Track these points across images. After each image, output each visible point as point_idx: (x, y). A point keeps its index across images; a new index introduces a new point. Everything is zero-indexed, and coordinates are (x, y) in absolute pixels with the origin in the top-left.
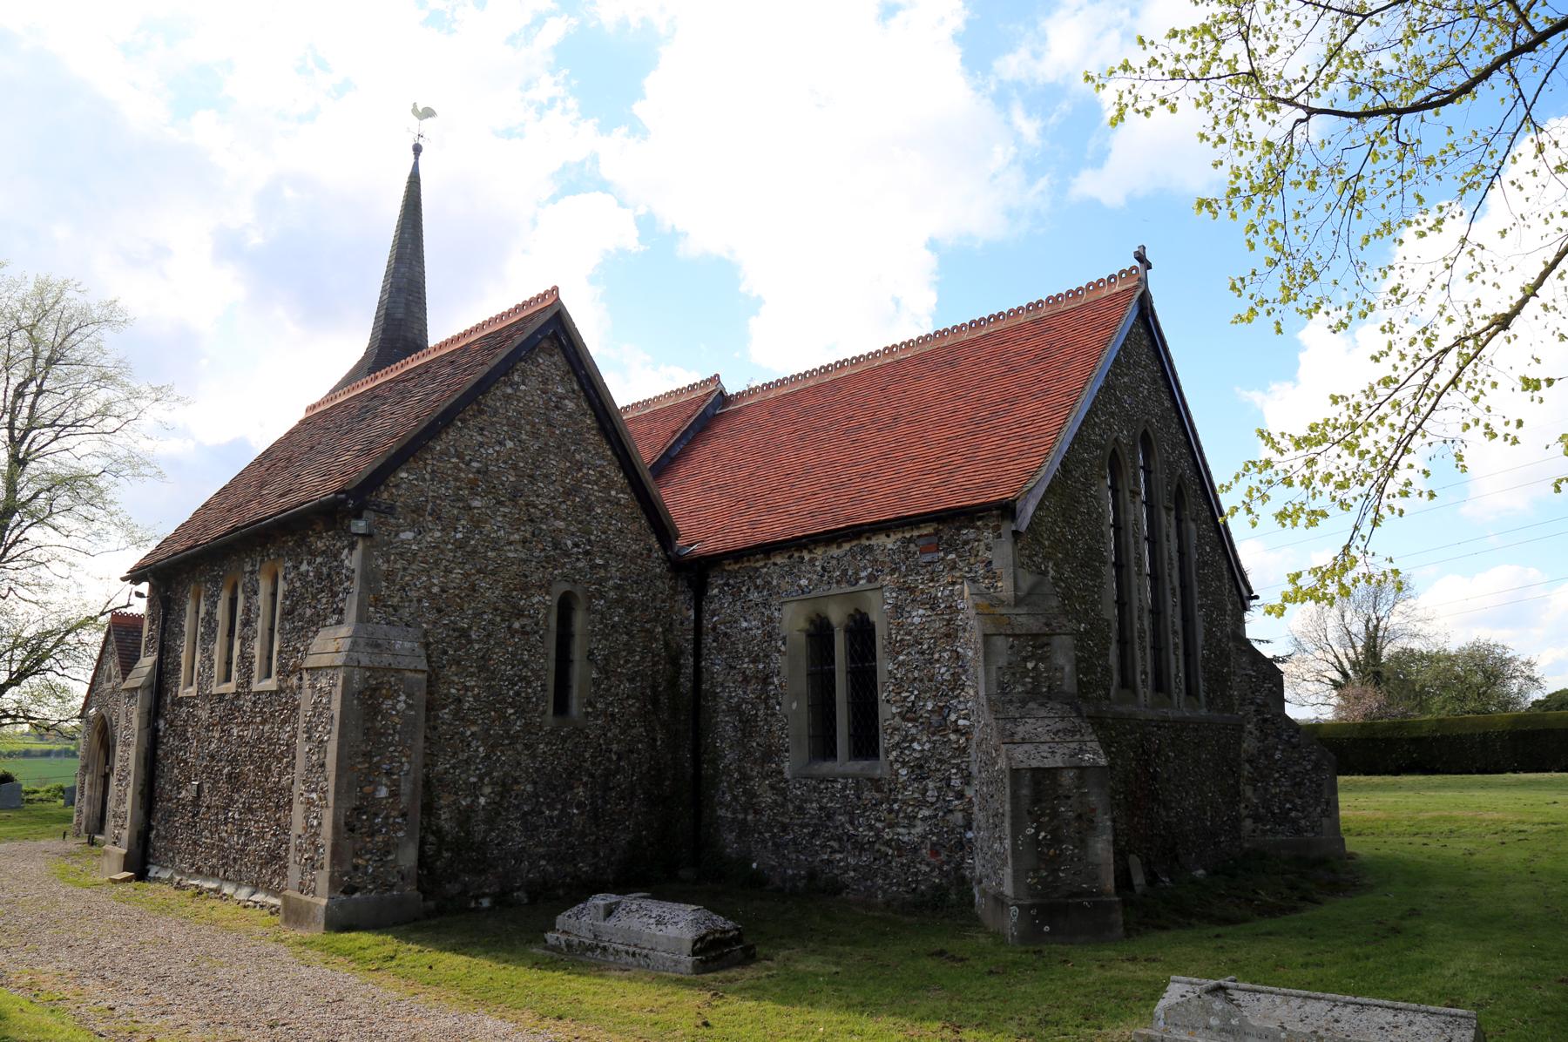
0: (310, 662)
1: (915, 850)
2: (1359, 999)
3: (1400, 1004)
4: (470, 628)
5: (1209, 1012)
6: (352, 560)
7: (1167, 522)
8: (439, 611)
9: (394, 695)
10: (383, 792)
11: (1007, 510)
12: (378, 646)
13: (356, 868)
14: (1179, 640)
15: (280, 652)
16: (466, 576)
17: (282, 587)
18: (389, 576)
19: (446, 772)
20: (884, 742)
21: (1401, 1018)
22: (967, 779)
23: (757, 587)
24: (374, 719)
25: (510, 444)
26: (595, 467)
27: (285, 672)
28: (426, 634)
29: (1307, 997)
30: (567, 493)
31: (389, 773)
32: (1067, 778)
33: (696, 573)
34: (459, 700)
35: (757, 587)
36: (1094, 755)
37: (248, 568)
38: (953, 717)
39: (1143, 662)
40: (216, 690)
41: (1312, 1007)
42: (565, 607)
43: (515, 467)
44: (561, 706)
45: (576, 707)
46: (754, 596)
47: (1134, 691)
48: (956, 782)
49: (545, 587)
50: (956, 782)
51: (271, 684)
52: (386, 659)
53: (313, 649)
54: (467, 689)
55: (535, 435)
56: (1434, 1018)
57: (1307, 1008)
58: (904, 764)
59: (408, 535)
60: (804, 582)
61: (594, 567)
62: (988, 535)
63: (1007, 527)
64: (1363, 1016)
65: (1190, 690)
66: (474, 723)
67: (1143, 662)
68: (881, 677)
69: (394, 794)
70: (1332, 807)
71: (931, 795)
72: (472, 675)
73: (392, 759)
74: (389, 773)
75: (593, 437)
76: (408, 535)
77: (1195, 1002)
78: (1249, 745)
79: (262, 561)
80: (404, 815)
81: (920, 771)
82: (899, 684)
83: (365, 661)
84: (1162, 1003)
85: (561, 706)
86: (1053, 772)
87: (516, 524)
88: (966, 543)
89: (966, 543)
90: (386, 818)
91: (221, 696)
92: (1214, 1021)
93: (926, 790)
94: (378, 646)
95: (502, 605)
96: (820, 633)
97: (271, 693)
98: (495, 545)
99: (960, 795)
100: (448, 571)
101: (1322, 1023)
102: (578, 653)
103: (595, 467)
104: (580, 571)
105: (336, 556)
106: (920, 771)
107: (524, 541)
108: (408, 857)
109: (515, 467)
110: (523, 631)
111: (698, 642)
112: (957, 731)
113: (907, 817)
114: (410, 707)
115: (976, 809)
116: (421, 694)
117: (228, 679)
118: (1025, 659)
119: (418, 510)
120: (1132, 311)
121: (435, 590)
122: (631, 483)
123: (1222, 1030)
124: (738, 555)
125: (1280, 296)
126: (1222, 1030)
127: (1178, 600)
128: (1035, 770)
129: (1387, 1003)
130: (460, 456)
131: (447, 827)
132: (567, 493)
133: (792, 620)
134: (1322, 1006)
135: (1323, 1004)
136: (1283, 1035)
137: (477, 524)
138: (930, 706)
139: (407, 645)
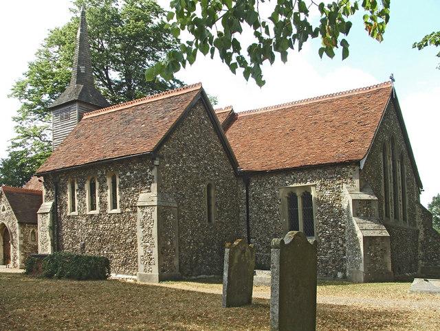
0: (138, 204)
1: (327, 262)
6: (154, 173)
7: (398, 165)
10: (169, 243)
11: (358, 163)
14: (401, 203)
15: (120, 201)
16: (183, 178)
17: (118, 181)
18: (164, 178)
20: (316, 231)
22: (344, 241)
23: (269, 183)
24: (165, 221)
25: (191, 136)
26: (214, 143)
27: (123, 207)
30: (207, 152)
33: (248, 177)
34: (184, 217)
35: (269, 183)
36: (386, 234)
37: (99, 173)
38: (340, 223)
39: (391, 209)
40: (89, 212)
42: (209, 187)
43: (193, 143)
44: (210, 220)
45: (213, 221)
46: (268, 186)
47: (389, 217)
48: (341, 242)
49: (203, 182)
50: (341, 242)
51: (118, 211)
53: (139, 200)
55: (197, 132)
58: (323, 237)
59: (168, 165)
60: (287, 182)
61: (216, 175)
62: (351, 170)
63: (357, 168)
65: (404, 219)
67: (391, 209)
68: (314, 212)
69: (171, 244)
71: (332, 246)
75: (212, 132)
76: (168, 165)
78: (421, 237)
79: (107, 171)
81: (328, 239)
82: (322, 214)
85: (210, 220)
87: (194, 162)
88: (344, 172)
89: (344, 172)
91: (92, 215)
93: (331, 244)
96: (292, 198)
97: (118, 214)
98: (189, 168)
99: (342, 246)
100: (179, 176)
102: (213, 203)
103: (214, 143)
104: (212, 177)
105: (145, 170)
106: (328, 239)
107: (197, 167)
108: (176, 262)
109: (193, 143)
110: (198, 196)
111: (247, 200)
112: (341, 227)
113: (324, 252)
115: (347, 250)
116: (176, 213)
117: (74, 210)
118: (364, 207)
119: (169, 157)
120: (388, 98)
122: (224, 148)
124: (262, 174)
127: (401, 190)
130: (178, 139)
132: (207, 152)
133: (282, 194)
137: (184, 162)
138: (332, 220)
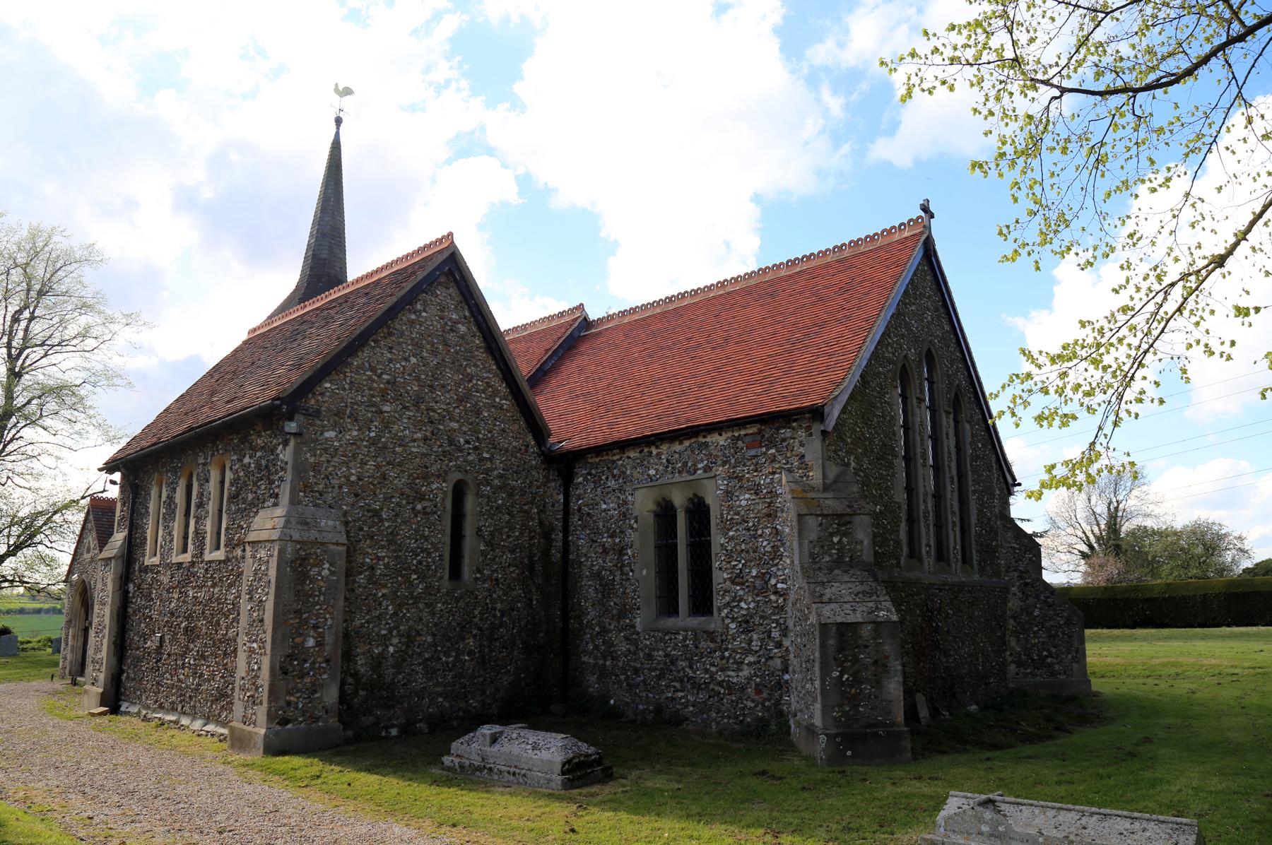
0: (252, 537)
1: (743, 689)
2: (1102, 810)
3: (1136, 814)
4: (381, 509)
5: (981, 821)
6: (286, 454)
7: (947, 423)
8: (356, 495)
9: (319, 564)
10: (311, 642)
11: (817, 413)
12: (306, 524)
13: (289, 704)
14: (957, 519)
15: (227, 529)
16: (378, 467)
17: (229, 476)
18: (316, 467)
19: (362, 626)
20: (718, 602)
21: (1137, 825)
22: (785, 632)
23: (614, 476)
24: (303, 583)
25: (413, 360)
26: (482, 379)
27: (231, 545)
28: (345, 514)
29: (1060, 809)
30: (460, 400)
31: (315, 627)
32: (866, 631)
33: (565, 465)
34: (372, 568)
35: (614, 476)
36: (887, 613)
37: (201, 461)
38: (773, 581)
39: (927, 537)
40: (175, 559)
41: (1064, 817)
42: (459, 492)
43: (418, 379)
44: (455, 572)
45: (467, 573)
46: (612, 483)
47: (920, 560)
48: (776, 634)
49: (442, 476)
50: (776, 634)
51: (220, 555)
52: (313, 534)
53: (254, 526)
54: (379, 559)
55: (434, 353)
56: (1163, 826)
57: (1060, 817)
58: (733, 620)
59: (331, 434)
60: (652, 472)
61: (482, 460)
62: (801, 434)
63: (817, 428)
64: (1106, 824)
65: (966, 560)
66: (385, 586)
67: (927, 537)
68: (715, 549)
69: (319, 644)
70: (1080, 655)
71: (755, 645)
72: (383, 547)
73: (318, 616)
74: (315, 627)
75: (481, 355)
76: (331, 434)
77: (970, 813)
78: (1013, 604)
79: (213, 455)
80: (327, 661)
81: (746, 625)
82: (729, 555)
83: (296, 536)
84: (942, 814)
85: (455, 572)
86: (854, 626)
87: (418, 425)
88: (784, 440)
89: (784, 440)
90: (313, 663)
91: (180, 565)
92: (985, 828)
93: (751, 641)
94: (306, 524)
95: (407, 491)
96: (665, 513)
97: (220, 562)
98: (402, 442)
99: (779, 645)
100: (363, 463)
101: (1073, 829)
102: (469, 530)
103: (482, 379)
104: (470, 463)
105: (273, 451)
106: (746, 625)
107: (425, 439)
108: (331, 695)
109: (418, 379)
110: (425, 512)
111: (566, 521)
112: (776, 593)
113: (735, 662)
114: (332, 573)
115: (791, 656)
116: (342, 563)
117: (185, 550)
118: (832, 535)
119: (339, 413)
120: (918, 253)
121: (353, 478)
122: (512, 392)
123: (992, 835)
124: (599, 450)
125: (1038, 240)
126: (992, 835)
127: (955, 486)
128: (840, 625)
129: (1125, 813)
130: (373, 370)
131: (362, 671)
132: (460, 400)
133: (643, 503)
134: (1072, 816)
135: (1073, 814)
136: (1041, 840)
137: (387, 425)
138: (754, 573)
139: (331, 523)
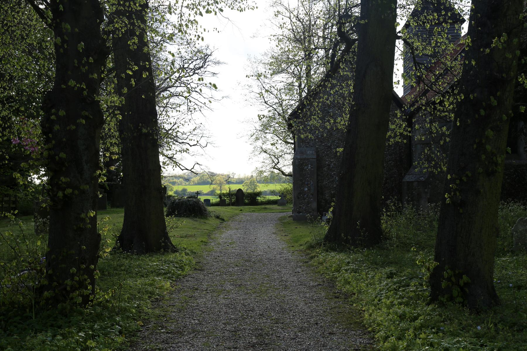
4: (331, 145)
8: (321, 142)
9: (307, 165)
10: (306, 189)
12: (303, 153)
13: (300, 207)
19: (326, 184)
28: (317, 148)
31: (307, 184)
32: (415, 184)
34: (329, 165)
52: (305, 156)
54: (331, 162)
66: (334, 171)
69: (309, 190)
70: (294, 184)
72: (333, 158)
73: (308, 181)
74: (307, 184)
80: (312, 195)
83: (299, 157)
86: (412, 182)
90: (307, 195)
94: (303, 153)
95: (341, 138)
114: (311, 168)
121: (320, 136)
125: (175, 156)
128: (408, 182)
131: (328, 198)
139: (311, 152)
